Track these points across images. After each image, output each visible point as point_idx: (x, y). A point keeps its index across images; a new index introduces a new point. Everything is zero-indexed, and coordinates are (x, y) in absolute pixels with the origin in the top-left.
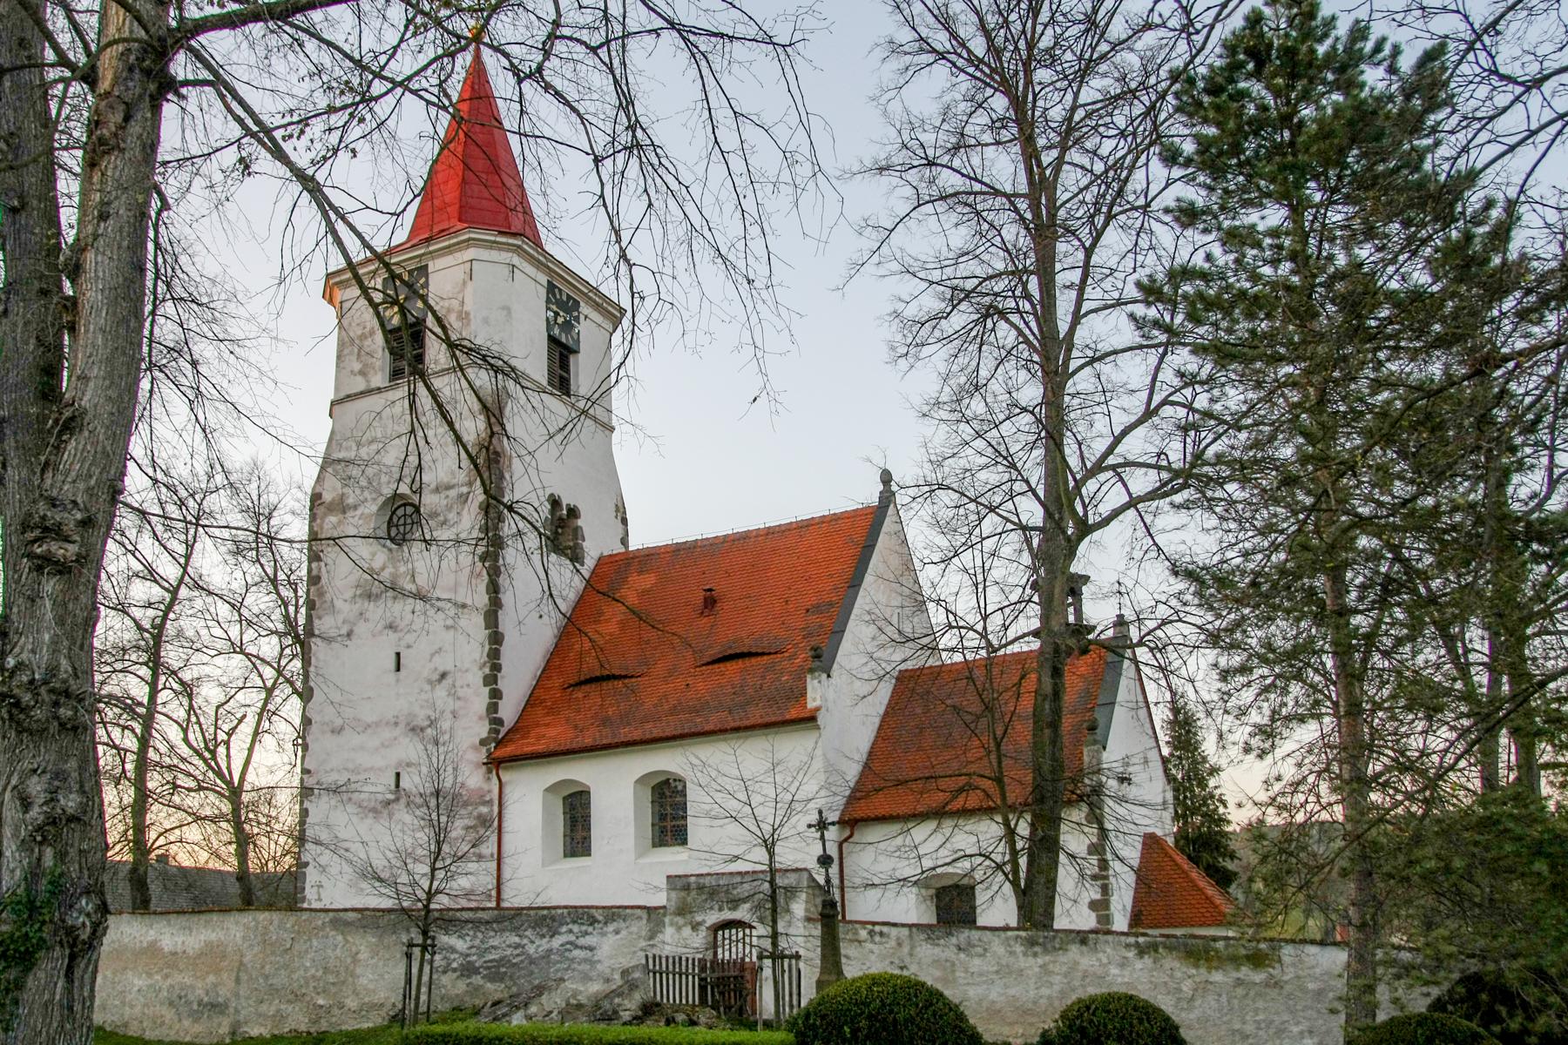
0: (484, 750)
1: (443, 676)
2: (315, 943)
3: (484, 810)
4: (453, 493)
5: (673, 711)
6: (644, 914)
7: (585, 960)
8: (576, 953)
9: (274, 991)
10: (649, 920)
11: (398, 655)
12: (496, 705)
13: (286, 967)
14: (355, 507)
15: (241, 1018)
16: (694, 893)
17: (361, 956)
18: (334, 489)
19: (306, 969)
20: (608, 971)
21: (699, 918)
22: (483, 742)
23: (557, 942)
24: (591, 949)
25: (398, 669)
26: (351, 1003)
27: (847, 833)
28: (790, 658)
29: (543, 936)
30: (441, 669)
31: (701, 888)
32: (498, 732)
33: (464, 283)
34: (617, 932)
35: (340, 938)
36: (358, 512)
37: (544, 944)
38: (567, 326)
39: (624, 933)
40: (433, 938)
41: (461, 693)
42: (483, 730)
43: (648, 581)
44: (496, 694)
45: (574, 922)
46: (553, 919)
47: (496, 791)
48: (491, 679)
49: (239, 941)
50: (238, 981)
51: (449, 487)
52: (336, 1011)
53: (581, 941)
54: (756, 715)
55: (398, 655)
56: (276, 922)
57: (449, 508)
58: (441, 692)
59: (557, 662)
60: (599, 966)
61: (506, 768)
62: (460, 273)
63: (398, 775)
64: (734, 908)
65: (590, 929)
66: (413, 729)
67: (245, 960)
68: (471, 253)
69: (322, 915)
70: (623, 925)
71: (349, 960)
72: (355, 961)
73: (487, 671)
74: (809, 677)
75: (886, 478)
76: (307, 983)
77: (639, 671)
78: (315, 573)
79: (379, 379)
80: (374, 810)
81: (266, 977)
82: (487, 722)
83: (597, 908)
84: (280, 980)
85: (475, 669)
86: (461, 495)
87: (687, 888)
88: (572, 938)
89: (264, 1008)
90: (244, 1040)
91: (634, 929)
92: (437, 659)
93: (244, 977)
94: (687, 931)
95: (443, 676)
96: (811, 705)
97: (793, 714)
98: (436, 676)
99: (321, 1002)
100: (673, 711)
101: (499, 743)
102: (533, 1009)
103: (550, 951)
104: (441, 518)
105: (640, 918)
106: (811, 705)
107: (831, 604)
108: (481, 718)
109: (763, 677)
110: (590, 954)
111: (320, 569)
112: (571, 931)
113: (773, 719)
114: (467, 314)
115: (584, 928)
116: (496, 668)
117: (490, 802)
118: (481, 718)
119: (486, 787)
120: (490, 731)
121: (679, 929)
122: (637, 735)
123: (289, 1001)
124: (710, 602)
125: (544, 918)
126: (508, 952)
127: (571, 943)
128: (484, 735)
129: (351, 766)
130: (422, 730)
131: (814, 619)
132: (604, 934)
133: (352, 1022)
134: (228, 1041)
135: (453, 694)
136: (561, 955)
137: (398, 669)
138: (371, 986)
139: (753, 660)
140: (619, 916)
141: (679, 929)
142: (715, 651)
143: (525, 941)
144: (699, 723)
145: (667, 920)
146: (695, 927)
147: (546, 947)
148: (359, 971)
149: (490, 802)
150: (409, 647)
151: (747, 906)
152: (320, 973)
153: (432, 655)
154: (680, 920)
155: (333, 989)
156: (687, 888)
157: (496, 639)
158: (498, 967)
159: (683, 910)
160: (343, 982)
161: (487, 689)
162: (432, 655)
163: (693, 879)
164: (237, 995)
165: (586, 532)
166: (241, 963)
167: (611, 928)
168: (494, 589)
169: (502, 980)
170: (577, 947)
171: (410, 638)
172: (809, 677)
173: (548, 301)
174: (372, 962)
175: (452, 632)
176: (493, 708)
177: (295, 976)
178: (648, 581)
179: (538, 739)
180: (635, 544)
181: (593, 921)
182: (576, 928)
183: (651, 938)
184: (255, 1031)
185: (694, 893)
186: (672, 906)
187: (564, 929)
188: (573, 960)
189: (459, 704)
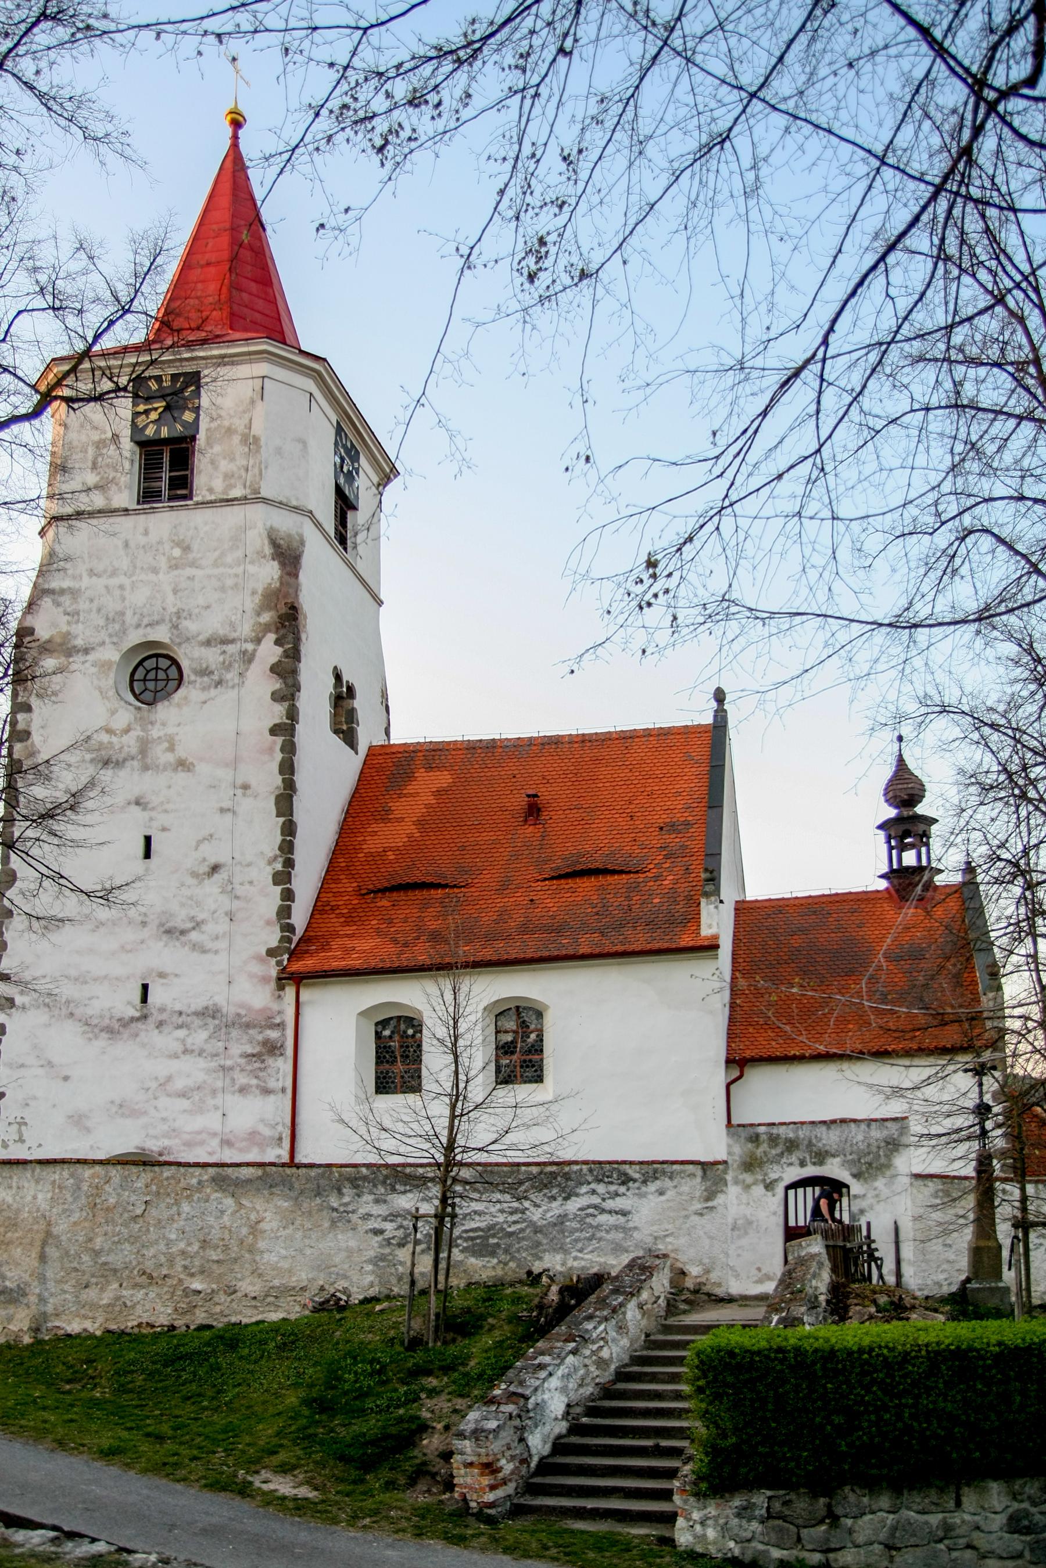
0: (273, 961)
1: (215, 868)
2: (186, 1207)
3: (273, 1034)
4: (231, 649)
5: (525, 929)
6: (699, 1172)
7: (616, 1228)
8: (603, 1218)
9: (108, 1272)
10: (704, 1176)
11: (148, 840)
12: (289, 907)
13: (133, 1239)
14: (86, 651)
15: (49, 1308)
16: (764, 1147)
17: (263, 1226)
18: (54, 624)
19: (169, 1243)
20: (649, 1240)
21: (773, 1176)
22: (271, 953)
23: (573, 1206)
24: (624, 1213)
25: (147, 855)
26: (249, 1286)
27: (737, 1074)
28: (656, 878)
29: (553, 1198)
30: (213, 860)
31: (774, 1140)
32: (290, 941)
33: (253, 402)
34: (661, 1193)
35: (229, 1201)
36: (90, 657)
37: (556, 1208)
38: (350, 477)
39: (670, 1194)
40: (453, 1205)
41: (240, 891)
42: (273, 938)
43: (443, 779)
44: (288, 895)
45: (599, 1181)
46: (567, 1177)
47: (290, 1011)
48: (283, 878)
49: (44, 1206)
50: (43, 1258)
51: (226, 641)
52: (222, 1297)
53: (610, 1204)
54: (640, 940)
55: (148, 840)
56: (116, 1180)
57: (228, 667)
58: (212, 887)
59: (342, 862)
60: (636, 1234)
61: (306, 985)
62: (246, 390)
63: (145, 988)
64: (821, 1163)
65: (622, 1189)
66: (169, 932)
67: (55, 1230)
68: (263, 368)
69: (198, 1171)
70: (668, 1183)
71: (244, 1231)
72: (254, 1229)
73: (279, 866)
74: (703, 901)
75: (720, 696)
76: (171, 1262)
77: (460, 880)
78: (20, 726)
79: (125, 496)
80: (109, 1030)
81: (97, 1253)
82: (277, 928)
83: (631, 1163)
84: (124, 1255)
85: (262, 863)
86: (245, 652)
87: (755, 1139)
88: (596, 1200)
89: (92, 1294)
90: (58, 1339)
91: (685, 1189)
92: (205, 847)
93: (52, 1252)
94: (759, 1190)
95: (215, 868)
96: (705, 931)
97: (686, 941)
98: (204, 868)
99: (197, 1285)
100: (525, 929)
101: (293, 954)
102: (645, 1295)
103: (563, 1218)
104: (216, 677)
105: (693, 1175)
106: (705, 931)
107: (687, 824)
108: (268, 923)
109: (629, 898)
110: (622, 1219)
111: (29, 723)
112: (594, 1192)
113: (666, 945)
114: (256, 440)
115: (612, 1188)
116: (289, 863)
117: (281, 1026)
118: (268, 923)
119: (275, 1007)
120: (282, 939)
121: (747, 1187)
122: (488, 954)
123: (136, 1286)
124: (534, 810)
125: (553, 1175)
126: (501, 1218)
127: (595, 1207)
128: (274, 943)
129: (73, 973)
130: (183, 932)
131: (669, 838)
132: (642, 1196)
133: (249, 1312)
134: (27, 1340)
135: (229, 890)
136: (582, 1221)
137: (147, 855)
138: (285, 1265)
139: (610, 878)
140: (664, 1173)
141: (747, 1187)
142: (559, 864)
143: (527, 1204)
144: (565, 944)
145: (729, 1177)
146: (769, 1186)
147: (560, 1211)
148: (261, 1245)
149: (281, 1026)
150: (164, 829)
151: (837, 1160)
152: (196, 1247)
153: (199, 843)
154: (748, 1178)
155: (217, 1269)
156: (755, 1139)
157: (289, 829)
158: (487, 1238)
159: (750, 1165)
160: (235, 1260)
161: (278, 889)
162: (199, 843)
163: (762, 1129)
164: (42, 1279)
165: (361, 715)
166: (48, 1234)
167: (652, 1187)
168: (288, 768)
169: (493, 1254)
170: (603, 1211)
171: (162, 819)
172: (703, 901)
173: (336, 444)
174: (282, 1233)
175: (229, 816)
176: (285, 912)
177: (150, 1252)
178: (443, 779)
179: (347, 951)
180: (397, 738)
181: (626, 1180)
182: (601, 1188)
183: (708, 1199)
184: (74, 1327)
185: (764, 1147)
186: (735, 1161)
187: (584, 1189)
188: (598, 1227)
189: (236, 904)
